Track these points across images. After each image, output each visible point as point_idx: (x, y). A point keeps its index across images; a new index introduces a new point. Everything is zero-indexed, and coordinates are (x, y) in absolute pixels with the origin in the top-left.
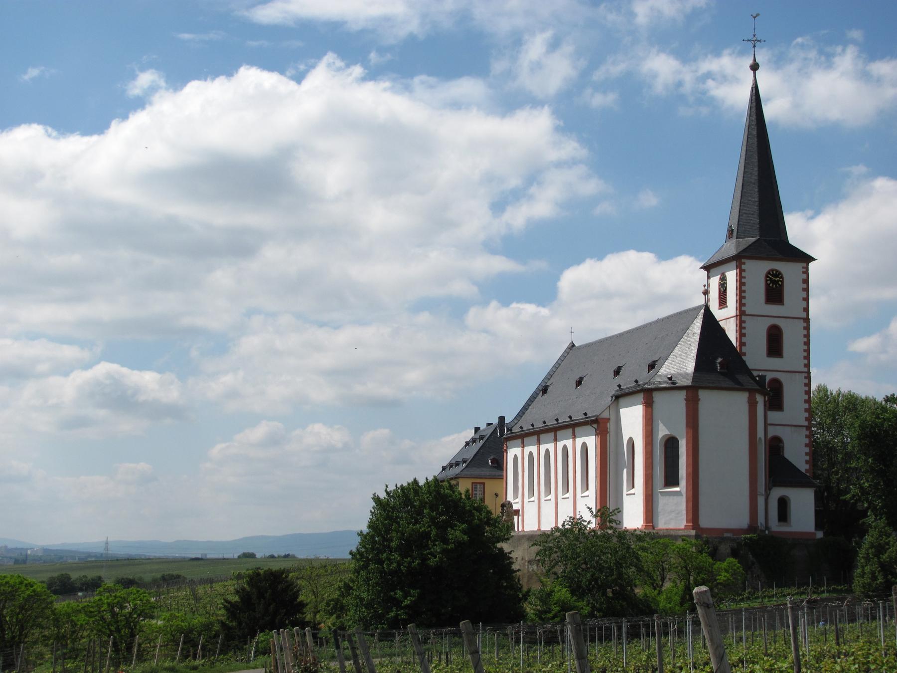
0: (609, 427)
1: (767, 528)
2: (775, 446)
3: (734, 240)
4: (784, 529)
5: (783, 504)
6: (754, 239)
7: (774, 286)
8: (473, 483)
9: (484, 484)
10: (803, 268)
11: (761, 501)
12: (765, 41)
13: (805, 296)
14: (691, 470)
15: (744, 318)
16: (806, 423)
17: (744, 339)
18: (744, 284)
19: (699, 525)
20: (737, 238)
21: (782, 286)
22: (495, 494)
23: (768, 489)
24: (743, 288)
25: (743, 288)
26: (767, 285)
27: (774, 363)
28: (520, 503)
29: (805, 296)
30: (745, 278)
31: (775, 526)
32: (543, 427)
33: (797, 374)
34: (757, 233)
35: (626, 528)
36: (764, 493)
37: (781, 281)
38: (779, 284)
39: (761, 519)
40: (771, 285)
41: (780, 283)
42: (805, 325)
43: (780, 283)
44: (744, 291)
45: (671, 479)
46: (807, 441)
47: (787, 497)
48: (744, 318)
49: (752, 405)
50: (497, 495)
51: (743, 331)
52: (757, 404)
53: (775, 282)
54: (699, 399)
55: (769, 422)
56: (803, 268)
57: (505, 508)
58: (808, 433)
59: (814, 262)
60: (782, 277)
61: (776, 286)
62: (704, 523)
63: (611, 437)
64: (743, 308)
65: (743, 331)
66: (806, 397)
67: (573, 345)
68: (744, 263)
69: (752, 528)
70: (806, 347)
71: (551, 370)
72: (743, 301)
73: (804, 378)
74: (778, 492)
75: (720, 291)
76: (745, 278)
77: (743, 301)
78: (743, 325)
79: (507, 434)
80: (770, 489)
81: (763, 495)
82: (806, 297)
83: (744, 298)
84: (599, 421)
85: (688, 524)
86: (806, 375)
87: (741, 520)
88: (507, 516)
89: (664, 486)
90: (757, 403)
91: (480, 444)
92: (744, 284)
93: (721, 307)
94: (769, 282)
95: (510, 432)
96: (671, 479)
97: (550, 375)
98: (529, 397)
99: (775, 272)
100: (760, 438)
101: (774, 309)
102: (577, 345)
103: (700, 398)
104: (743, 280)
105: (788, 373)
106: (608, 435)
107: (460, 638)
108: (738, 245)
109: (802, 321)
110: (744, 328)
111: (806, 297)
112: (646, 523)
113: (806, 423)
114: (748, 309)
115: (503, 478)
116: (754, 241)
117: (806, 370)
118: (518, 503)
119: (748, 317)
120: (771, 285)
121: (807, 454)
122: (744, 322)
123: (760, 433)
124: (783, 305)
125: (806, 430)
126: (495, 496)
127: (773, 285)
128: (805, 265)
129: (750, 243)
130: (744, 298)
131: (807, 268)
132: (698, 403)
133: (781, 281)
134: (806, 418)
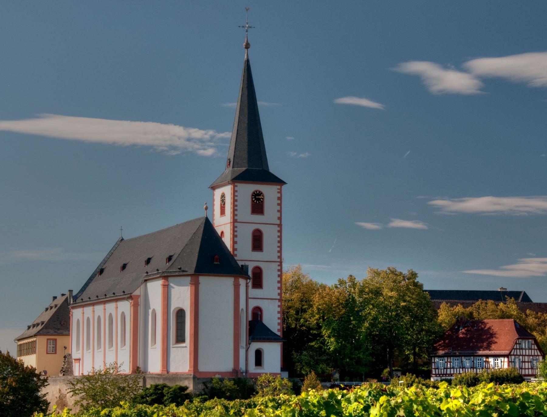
0: (139, 301)
1: (247, 371)
2: (257, 312)
3: (231, 168)
4: (258, 370)
5: (259, 354)
6: (244, 169)
7: (258, 202)
8: (48, 339)
9: (56, 340)
10: (278, 189)
11: (242, 352)
12: (254, 27)
13: (279, 209)
14: (193, 332)
15: (236, 224)
16: (279, 297)
17: (236, 239)
18: (236, 201)
19: (198, 370)
20: (233, 168)
21: (262, 202)
22: (64, 347)
23: (248, 344)
24: (236, 203)
25: (236, 203)
26: (253, 201)
27: (257, 255)
28: (81, 354)
29: (279, 209)
30: (237, 196)
31: (253, 369)
32: (96, 300)
33: (273, 263)
34: (247, 165)
35: (149, 372)
36: (245, 347)
37: (263, 199)
38: (261, 201)
39: (242, 366)
40: (255, 201)
41: (262, 200)
42: (279, 229)
43: (262, 200)
44: (236, 206)
45: (180, 339)
46: (279, 309)
47: (260, 348)
48: (236, 224)
49: (237, 287)
50: (65, 348)
51: (235, 233)
52: (240, 286)
53: (259, 199)
54: (200, 283)
55: (250, 296)
56: (278, 189)
57: (66, 359)
58: (279, 304)
59: (286, 185)
60: (263, 196)
61: (259, 202)
62: (202, 368)
63: (141, 309)
64: (236, 218)
65: (235, 233)
66: (279, 279)
67: (122, 239)
68: (237, 186)
69: (236, 371)
70: (279, 245)
71: (106, 257)
72: (236, 212)
73: (277, 266)
74: (255, 346)
75: (221, 205)
76: (237, 196)
77: (236, 212)
78: (236, 229)
79: (73, 304)
80: (250, 344)
81: (244, 348)
82: (279, 209)
83: (237, 210)
84: (133, 297)
85: (191, 369)
86: (279, 263)
87: (227, 366)
88: (68, 364)
89: (175, 343)
90: (240, 285)
91: (54, 310)
92: (236, 201)
93: (222, 216)
94: (254, 199)
95: (74, 303)
96: (180, 339)
97: (105, 261)
98: (92, 274)
99: (258, 192)
100: (242, 309)
101: (257, 218)
102: (125, 238)
103: (200, 282)
104: (236, 198)
105: (266, 263)
106: (139, 307)
107: (457, 409)
108: (233, 172)
109: (277, 226)
110: (236, 231)
111: (279, 209)
112: (163, 369)
113: (279, 297)
114: (238, 218)
115: (69, 335)
116: (244, 170)
117: (279, 260)
118: (80, 353)
119: (239, 224)
120: (255, 201)
121: (279, 318)
122: (236, 227)
123: (242, 305)
124: (264, 215)
125: (279, 302)
126: (64, 348)
127: (256, 202)
128: (279, 187)
129: (241, 172)
130: (237, 210)
131: (281, 189)
132: (199, 286)
133: (263, 199)
134: (278, 293)
